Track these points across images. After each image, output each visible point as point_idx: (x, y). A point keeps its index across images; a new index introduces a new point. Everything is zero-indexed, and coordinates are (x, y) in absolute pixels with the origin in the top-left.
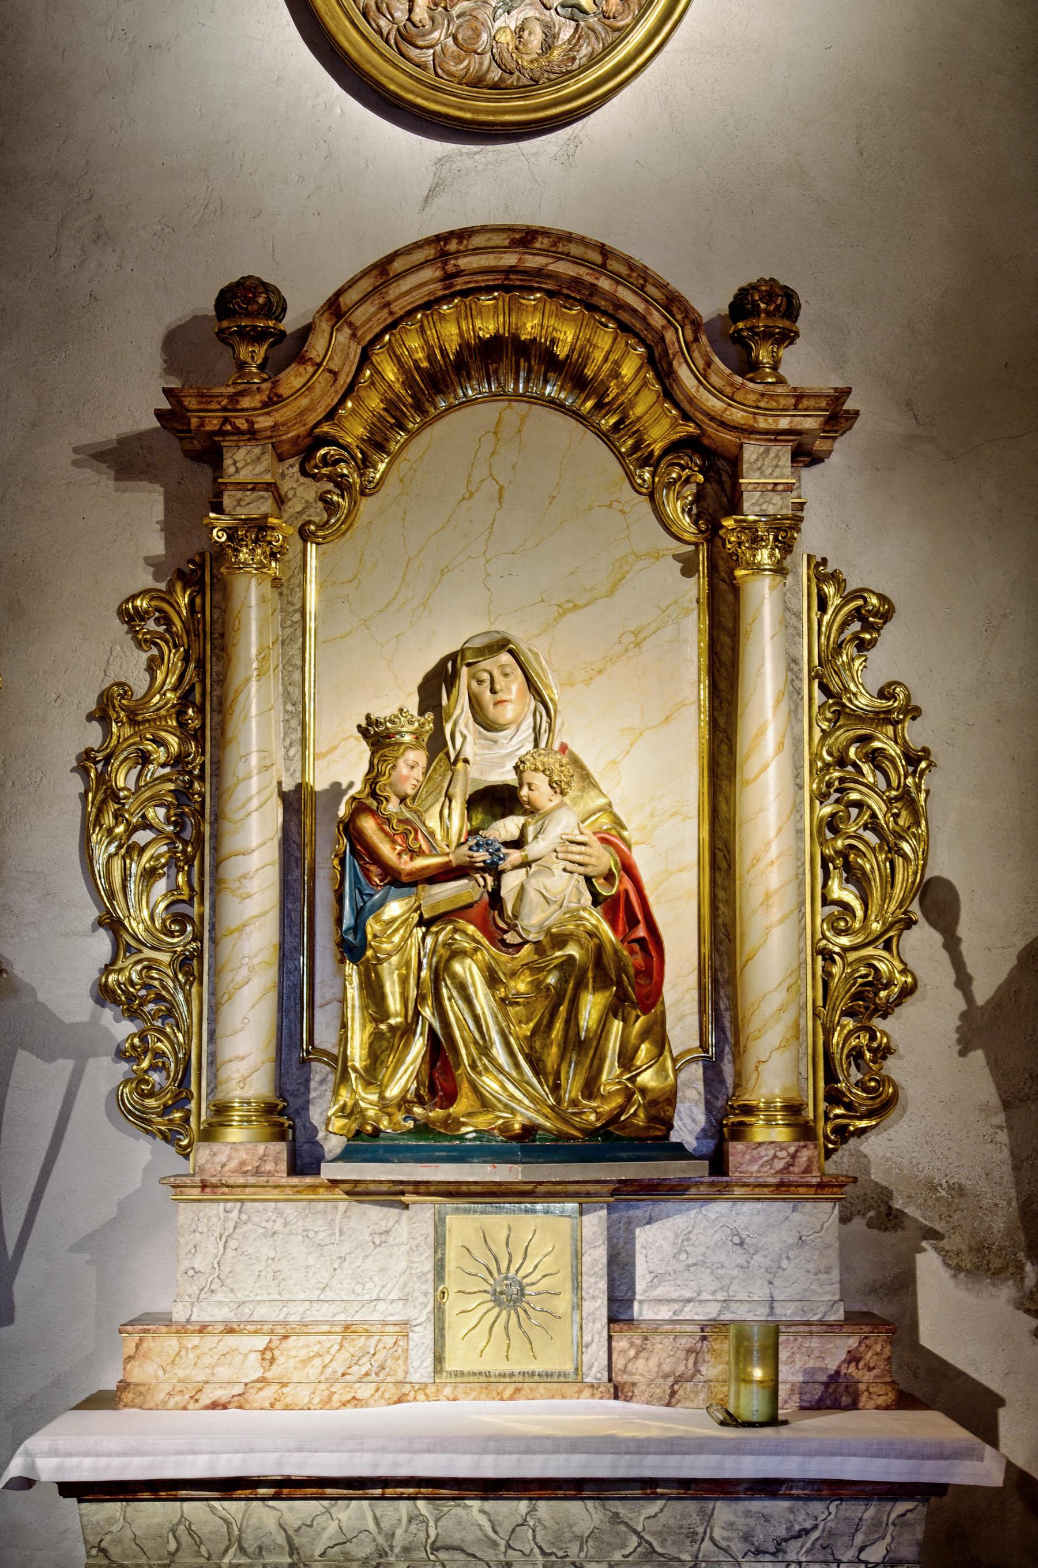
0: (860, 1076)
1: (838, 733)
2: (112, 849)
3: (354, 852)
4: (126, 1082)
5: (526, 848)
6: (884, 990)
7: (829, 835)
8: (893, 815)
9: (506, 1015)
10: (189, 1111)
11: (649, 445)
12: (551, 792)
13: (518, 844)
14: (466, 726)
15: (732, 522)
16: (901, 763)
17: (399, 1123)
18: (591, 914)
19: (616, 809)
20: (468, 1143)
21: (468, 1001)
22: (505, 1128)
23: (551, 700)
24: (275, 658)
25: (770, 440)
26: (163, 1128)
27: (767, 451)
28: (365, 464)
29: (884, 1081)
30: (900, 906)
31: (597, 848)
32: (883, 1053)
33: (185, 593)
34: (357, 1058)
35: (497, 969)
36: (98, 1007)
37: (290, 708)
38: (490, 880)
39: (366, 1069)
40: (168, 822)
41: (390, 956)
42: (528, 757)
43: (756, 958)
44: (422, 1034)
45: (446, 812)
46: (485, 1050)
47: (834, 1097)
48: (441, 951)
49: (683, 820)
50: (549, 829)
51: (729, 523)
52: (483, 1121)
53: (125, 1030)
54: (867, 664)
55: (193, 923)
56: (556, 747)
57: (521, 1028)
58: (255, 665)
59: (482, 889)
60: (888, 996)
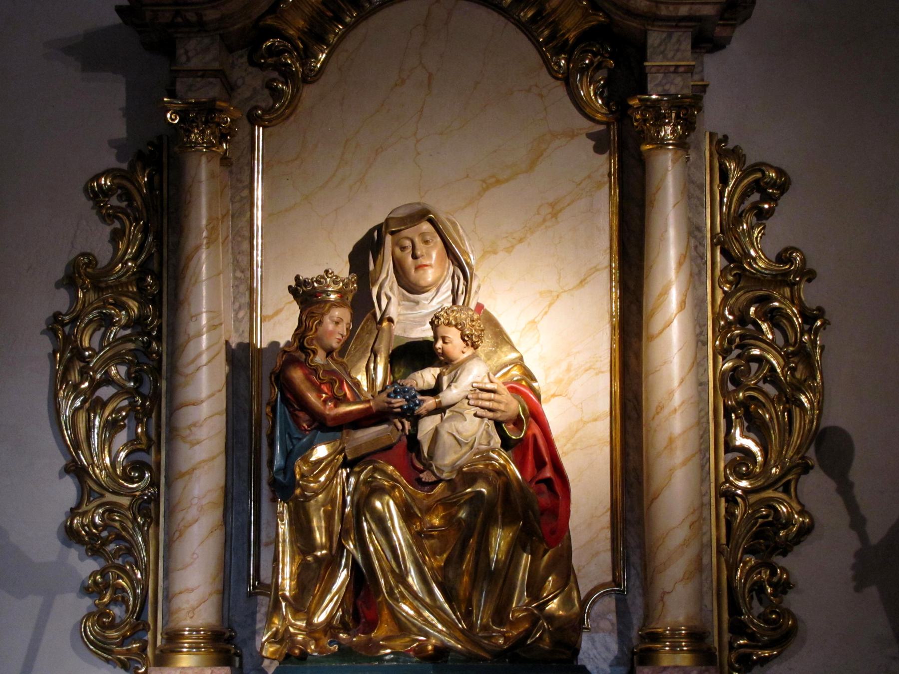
0: (762, 609)
1: (738, 294)
2: (78, 403)
3: (284, 400)
4: (88, 616)
5: (441, 395)
6: (783, 529)
7: (731, 387)
8: (790, 369)
9: (421, 548)
10: (146, 641)
11: (564, 35)
12: (463, 344)
13: (435, 391)
14: (391, 289)
15: (637, 101)
16: (798, 321)
17: (325, 647)
18: (500, 455)
19: (528, 363)
20: (386, 663)
21: (386, 533)
22: (420, 650)
23: (468, 264)
24: (224, 230)
25: (672, 27)
26: (122, 657)
27: (670, 35)
28: (307, 55)
29: (786, 613)
30: (798, 451)
31: (506, 396)
32: (783, 587)
33: (145, 172)
34: (288, 588)
35: (413, 504)
36: (65, 548)
37: (239, 274)
38: (407, 424)
39: (295, 597)
40: (129, 378)
41: (317, 494)
42: (442, 313)
43: (661, 496)
44: (346, 566)
45: (372, 366)
46: (402, 578)
47: (738, 628)
48: (363, 488)
49: (597, 374)
50: (462, 377)
51: (634, 102)
52: (399, 644)
53: (91, 565)
54: (767, 231)
55: (150, 470)
56: (473, 305)
57: (435, 559)
58: (205, 234)
59: (400, 433)
60: (787, 535)
